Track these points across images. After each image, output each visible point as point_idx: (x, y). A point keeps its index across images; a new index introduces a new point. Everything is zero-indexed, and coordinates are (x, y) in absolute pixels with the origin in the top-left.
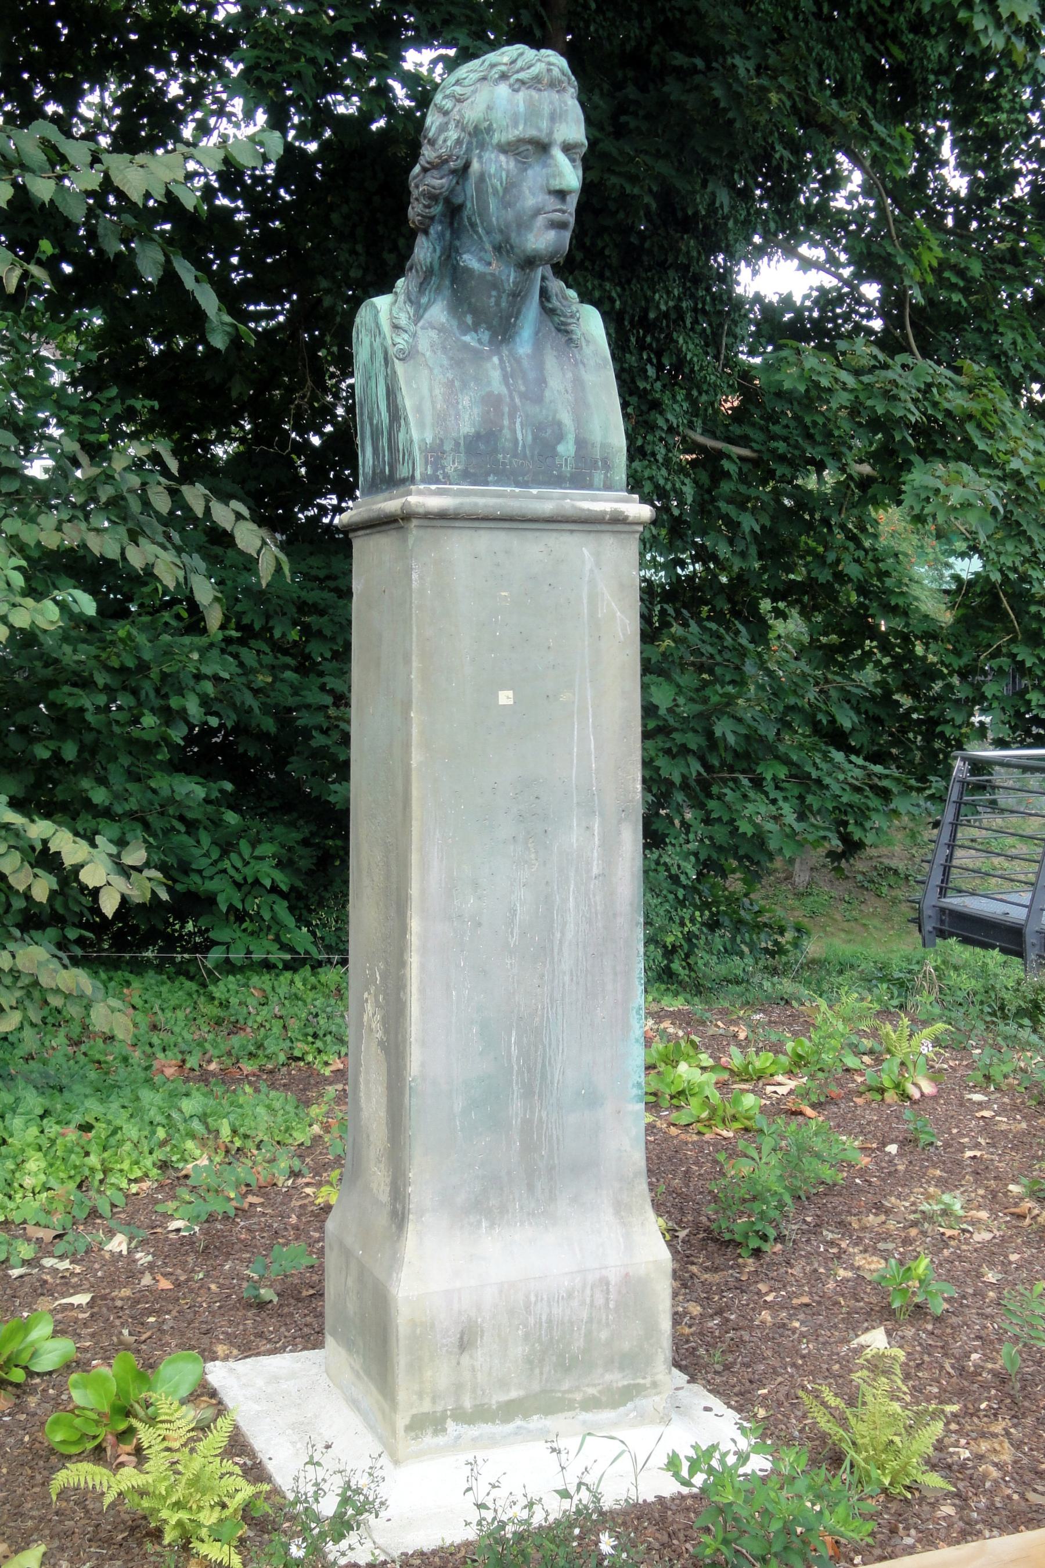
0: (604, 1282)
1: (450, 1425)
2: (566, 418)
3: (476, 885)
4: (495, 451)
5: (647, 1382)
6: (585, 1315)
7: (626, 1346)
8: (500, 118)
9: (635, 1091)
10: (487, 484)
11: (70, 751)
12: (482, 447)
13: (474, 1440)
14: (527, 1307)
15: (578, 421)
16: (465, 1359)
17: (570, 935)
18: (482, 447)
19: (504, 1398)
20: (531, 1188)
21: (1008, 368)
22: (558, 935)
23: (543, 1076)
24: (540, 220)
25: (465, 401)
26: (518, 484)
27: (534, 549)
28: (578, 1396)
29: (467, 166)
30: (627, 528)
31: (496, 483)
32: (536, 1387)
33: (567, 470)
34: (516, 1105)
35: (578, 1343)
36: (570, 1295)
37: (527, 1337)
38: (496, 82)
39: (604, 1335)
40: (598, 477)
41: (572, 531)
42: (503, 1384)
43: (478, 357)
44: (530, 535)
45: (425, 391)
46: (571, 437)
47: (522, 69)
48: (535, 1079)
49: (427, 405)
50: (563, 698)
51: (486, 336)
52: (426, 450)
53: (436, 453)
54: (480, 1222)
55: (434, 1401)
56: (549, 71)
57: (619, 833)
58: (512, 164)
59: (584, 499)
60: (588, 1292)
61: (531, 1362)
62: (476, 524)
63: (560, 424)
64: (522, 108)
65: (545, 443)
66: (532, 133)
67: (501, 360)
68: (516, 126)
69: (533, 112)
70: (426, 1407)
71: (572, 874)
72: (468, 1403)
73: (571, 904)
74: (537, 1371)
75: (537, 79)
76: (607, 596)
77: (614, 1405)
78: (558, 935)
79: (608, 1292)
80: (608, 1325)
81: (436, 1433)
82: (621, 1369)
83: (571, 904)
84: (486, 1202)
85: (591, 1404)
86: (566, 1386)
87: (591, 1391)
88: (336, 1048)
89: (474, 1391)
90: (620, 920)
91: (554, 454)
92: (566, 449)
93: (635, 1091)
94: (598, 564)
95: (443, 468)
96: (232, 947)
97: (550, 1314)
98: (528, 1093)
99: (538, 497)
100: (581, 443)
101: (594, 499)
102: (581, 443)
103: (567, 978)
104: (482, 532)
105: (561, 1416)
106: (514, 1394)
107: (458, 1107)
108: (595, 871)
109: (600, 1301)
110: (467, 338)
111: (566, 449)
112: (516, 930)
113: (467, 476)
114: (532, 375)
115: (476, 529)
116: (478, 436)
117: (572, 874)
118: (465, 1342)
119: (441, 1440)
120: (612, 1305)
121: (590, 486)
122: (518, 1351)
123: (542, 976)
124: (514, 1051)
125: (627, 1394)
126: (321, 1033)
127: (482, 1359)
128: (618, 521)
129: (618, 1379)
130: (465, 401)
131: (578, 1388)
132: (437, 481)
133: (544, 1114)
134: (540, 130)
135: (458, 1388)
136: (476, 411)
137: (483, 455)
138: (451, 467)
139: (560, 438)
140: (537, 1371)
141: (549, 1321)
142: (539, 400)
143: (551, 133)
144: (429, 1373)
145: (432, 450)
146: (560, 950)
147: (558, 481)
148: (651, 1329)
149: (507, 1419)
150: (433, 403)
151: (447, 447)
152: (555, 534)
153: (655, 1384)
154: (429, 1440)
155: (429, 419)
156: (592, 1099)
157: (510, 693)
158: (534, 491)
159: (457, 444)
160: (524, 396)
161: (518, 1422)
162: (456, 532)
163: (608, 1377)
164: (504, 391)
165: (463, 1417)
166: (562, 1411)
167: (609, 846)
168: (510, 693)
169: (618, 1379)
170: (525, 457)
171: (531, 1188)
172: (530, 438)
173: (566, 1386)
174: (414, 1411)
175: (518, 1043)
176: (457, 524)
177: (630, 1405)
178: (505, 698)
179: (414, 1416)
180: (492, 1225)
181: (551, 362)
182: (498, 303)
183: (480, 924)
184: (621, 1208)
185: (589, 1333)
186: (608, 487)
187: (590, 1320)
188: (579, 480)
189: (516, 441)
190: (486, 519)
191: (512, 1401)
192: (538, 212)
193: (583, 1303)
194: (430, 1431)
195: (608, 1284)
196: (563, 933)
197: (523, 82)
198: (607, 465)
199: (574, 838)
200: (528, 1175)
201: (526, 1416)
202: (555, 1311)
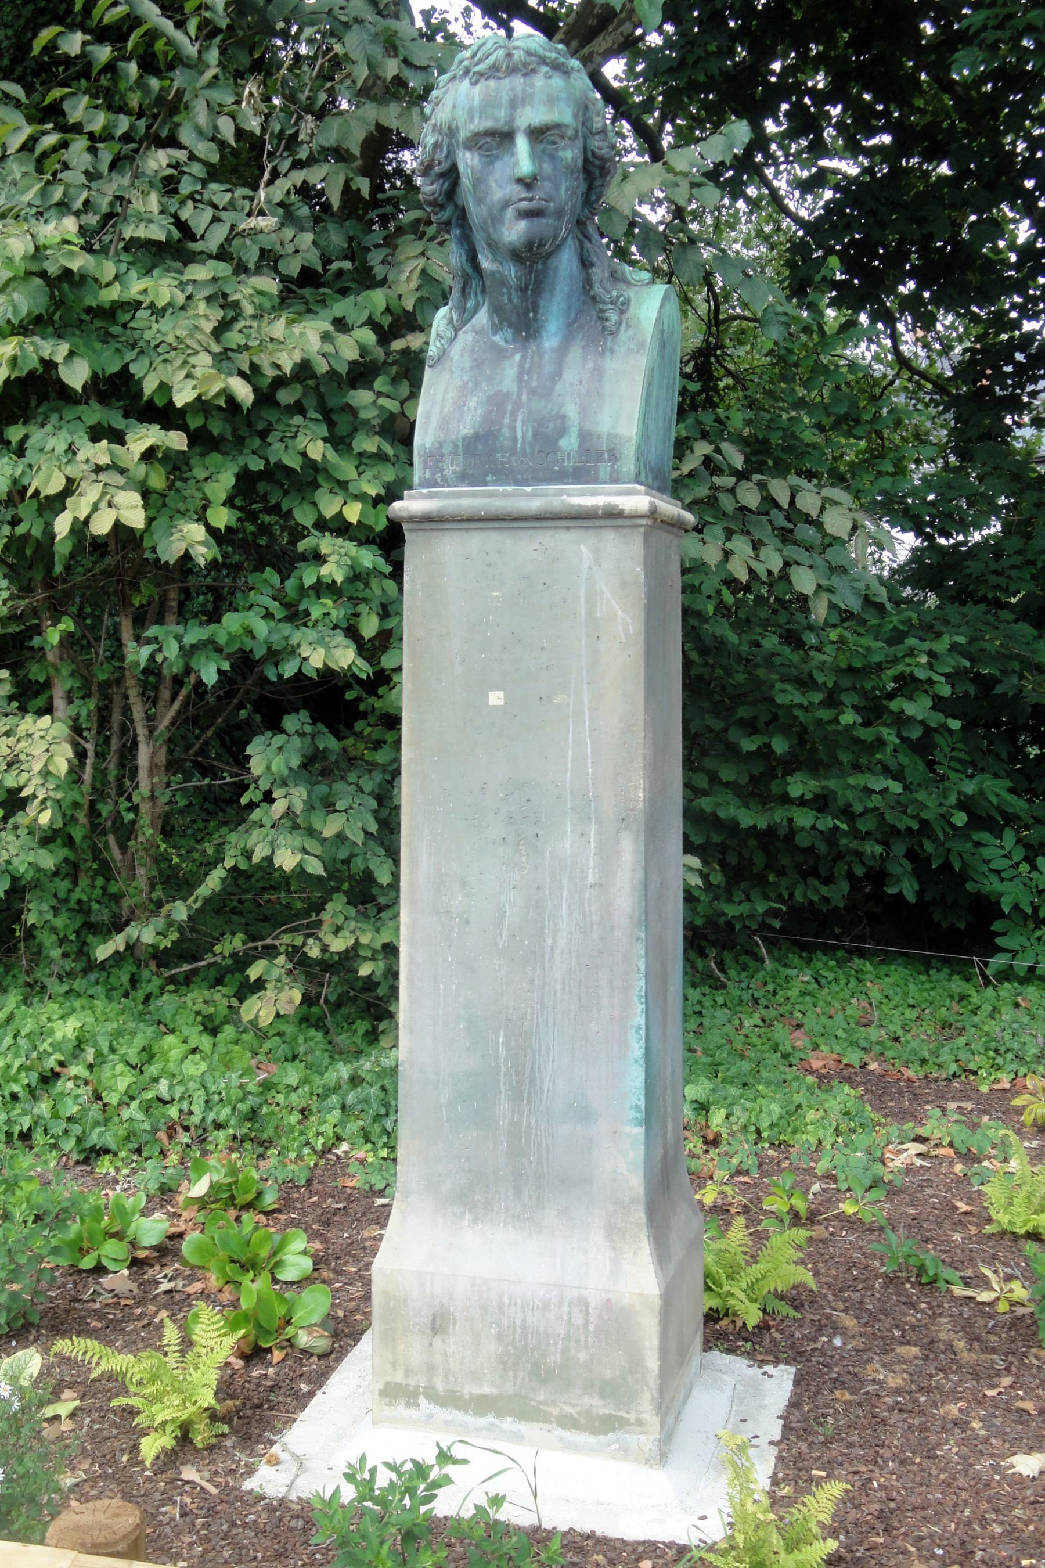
0: (583, 1304)
1: (422, 1400)
2: (571, 411)
3: (464, 883)
5: (632, 1417)
6: (562, 1331)
7: (608, 1374)
9: (633, 1114)
10: (485, 484)
11: (780, 746)
12: (480, 447)
13: (447, 1423)
14: (501, 1307)
15: (583, 411)
16: (437, 1342)
17: (562, 943)
18: (480, 447)
19: (476, 1391)
20: (518, 1191)
22: (549, 941)
23: (532, 1082)
24: (510, 212)
25: (472, 402)
26: (517, 483)
27: (526, 548)
28: (555, 1411)
29: (454, 168)
30: (628, 522)
31: (495, 483)
32: (509, 1389)
33: (569, 465)
34: (504, 1107)
35: (555, 1357)
36: (546, 1307)
37: (500, 1336)
39: (583, 1356)
40: (604, 470)
41: (568, 528)
42: (476, 1377)
43: (500, 354)
44: (523, 534)
45: (439, 397)
46: (574, 431)
47: (480, 61)
48: (524, 1085)
50: (558, 699)
51: (509, 334)
53: (435, 457)
54: (463, 1214)
55: (407, 1375)
56: (509, 55)
57: (618, 842)
58: (477, 159)
59: (583, 493)
60: (566, 1308)
61: (505, 1363)
62: (466, 525)
63: (564, 418)
64: (476, 101)
65: (545, 439)
66: (489, 124)
67: (524, 358)
68: (472, 119)
69: (489, 103)
70: (399, 1378)
71: (565, 881)
72: (440, 1386)
73: (564, 911)
74: (511, 1373)
75: (495, 67)
77: (595, 1431)
78: (549, 941)
79: (587, 1313)
80: (586, 1347)
81: (408, 1405)
82: (602, 1395)
83: (564, 911)
84: (469, 1197)
85: (568, 1422)
86: (541, 1396)
87: (569, 1409)
88: (1014, 1067)
89: (446, 1375)
90: (617, 933)
91: (556, 449)
92: (569, 443)
93: (633, 1114)
94: (597, 561)
95: (442, 471)
96: (1020, 955)
97: (524, 1321)
98: (517, 1095)
99: (532, 495)
100: (585, 436)
101: (594, 493)
102: (585, 436)
103: (559, 986)
104: (473, 533)
105: (537, 1426)
106: (486, 1390)
107: (444, 1100)
108: (591, 879)
109: (578, 1320)
110: (497, 339)
111: (569, 443)
112: (505, 932)
113: (464, 478)
114: (548, 369)
115: (467, 530)
116: (476, 437)
117: (565, 881)
118: (438, 1324)
119: (413, 1413)
120: (591, 1328)
121: (596, 481)
122: (491, 1348)
123: (532, 982)
124: (502, 1052)
125: (607, 1425)
126: (1002, 1050)
127: (453, 1347)
128: (612, 516)
129: (601, 1407)
130: (472, 402)
131: (554, 1403)
132: (436, 485)
133: (533, 1120)
134: (496, 120)
135: (431, 1369)
136: (479, 411)
137: (482, 456)
138: (450, 469)
139: (563, 432)
140: (511, 1373)
141: (524, 1328)
143: (511, 120)
144: (402, 1347)
145: (431, 454)
146: (552, 957)
147: (561, 477)
148: (636, 1364)
149: (480, 1412)
150: (443, 407)
151: (446, 450)
152: (550, 532)
153: (640, 1422)
154: (401, 1409)
156: (585, 1115)
157: (501, 694)
158: (528, 489)
159: (456, 446)
160: (533, 392)
161: (491, 1419)
162: (447, 534)
163: (587, 1400)
164: (515, 388)
165: (432, 1396)
166: (532, 1420)
167: (607, 855)
168: (501, 694)
169: (601, 1407)
170: (525, 454)
171: (518, 1191)
172: (530, 434)
173: (541, 1396)
174: (388, 1379)
176: (447, 526)
177: (611, 1436)
178: (496, 698)
179: (388, 1383)
180: (475, 1220)
182: (510, 300)
183: (467, 922)
184: (612, 1231)
185: (565, 1351)
186: (615, 480)
187: (568, 1338)
188: (582, 473)
189: (515, 439)
190: (470, 519)
191: (485, 1396)
192: (506, 204)
193: (559, 1318)
194: (403, 1402)
195: (587, 1305)
196: (555, 941)
197: (481, 75)
198: (613, 456)
200: (520, 1179)
201: (500, 1415)
202: (529, 1318)
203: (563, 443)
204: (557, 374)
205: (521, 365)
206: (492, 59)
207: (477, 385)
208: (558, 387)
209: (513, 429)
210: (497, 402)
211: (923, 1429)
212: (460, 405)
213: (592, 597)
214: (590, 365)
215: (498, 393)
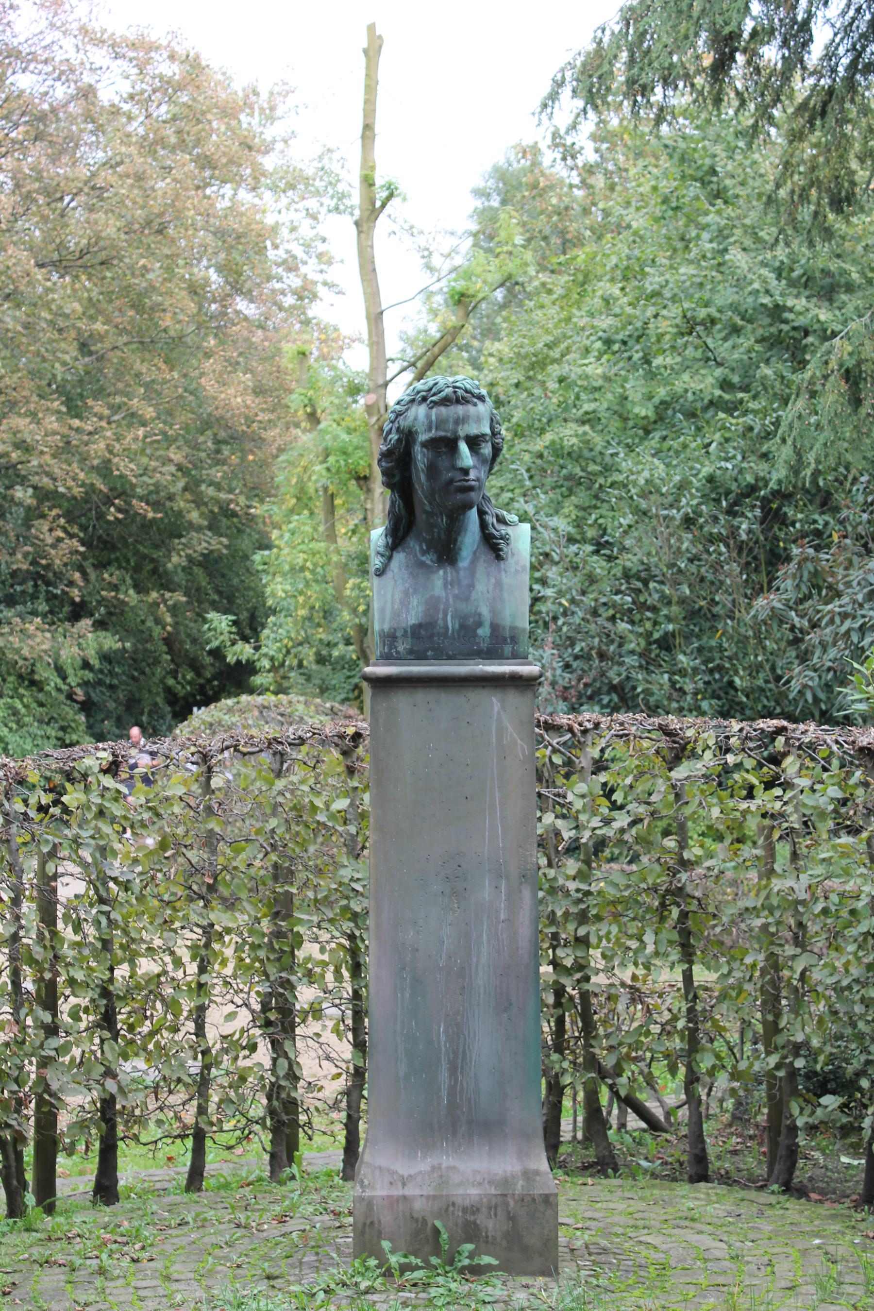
2: (485, 611)
4: (432, 636)
8: (420, 427)
17: (483, 960)
18: (423, 632)
21: (164, 122)
23: (464, 1052)
27: (447, 702)
38: (420, 403)
45: (389, 597)
46: (487, 624)
49: (389, 607)
52: (384, 636)
63: (480, 615)
76: (511, 729)
92: (484, 632)
94: (503, 708)
100: (494, 627)
102: (494, 627)
110: (423, 558)
111: (484, 632)
114: (465, 582)
116: (420, 626)
124: (443, 1038)
138: (402, 647)
139: (480, 624)
142: (467, 599)
151: (399, 634)
155: (388, 615)
159: (406, 632)
167: (513, 901)
175: (446, 1032)
181: (481, 567)
199: (486, 893)
203: (480, 631)
204: (472, 586)
205: (445, 579)
206: (443, 394)
207: (416, 591)
208: (474, 594)
209: (445, 620)
210: (433, 604)
211: (705, 662)
212: (405, 603)
213: (500, 730)
214: (493, 580)
215: (432, 597)
